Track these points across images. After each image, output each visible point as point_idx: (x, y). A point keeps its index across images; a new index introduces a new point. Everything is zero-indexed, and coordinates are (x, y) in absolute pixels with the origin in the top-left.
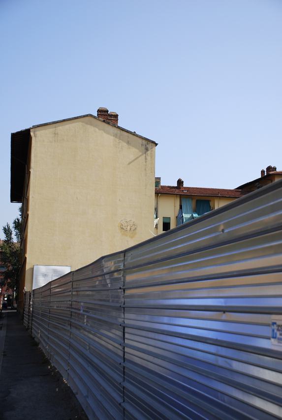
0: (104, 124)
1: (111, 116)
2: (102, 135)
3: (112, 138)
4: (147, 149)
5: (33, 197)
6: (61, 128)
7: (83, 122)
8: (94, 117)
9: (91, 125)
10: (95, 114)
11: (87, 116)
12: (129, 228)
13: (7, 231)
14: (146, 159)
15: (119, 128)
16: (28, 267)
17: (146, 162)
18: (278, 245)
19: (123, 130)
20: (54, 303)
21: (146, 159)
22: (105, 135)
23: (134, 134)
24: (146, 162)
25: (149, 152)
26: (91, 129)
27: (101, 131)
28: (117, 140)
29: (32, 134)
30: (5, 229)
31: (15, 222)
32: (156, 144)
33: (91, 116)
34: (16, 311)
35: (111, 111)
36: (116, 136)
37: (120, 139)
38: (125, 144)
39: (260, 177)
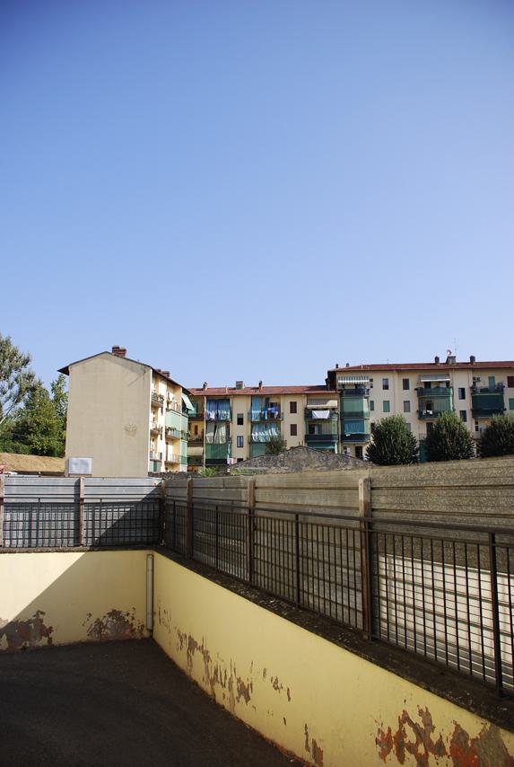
2: (114, 367)
3: (120, 367)
36: (123, 365)
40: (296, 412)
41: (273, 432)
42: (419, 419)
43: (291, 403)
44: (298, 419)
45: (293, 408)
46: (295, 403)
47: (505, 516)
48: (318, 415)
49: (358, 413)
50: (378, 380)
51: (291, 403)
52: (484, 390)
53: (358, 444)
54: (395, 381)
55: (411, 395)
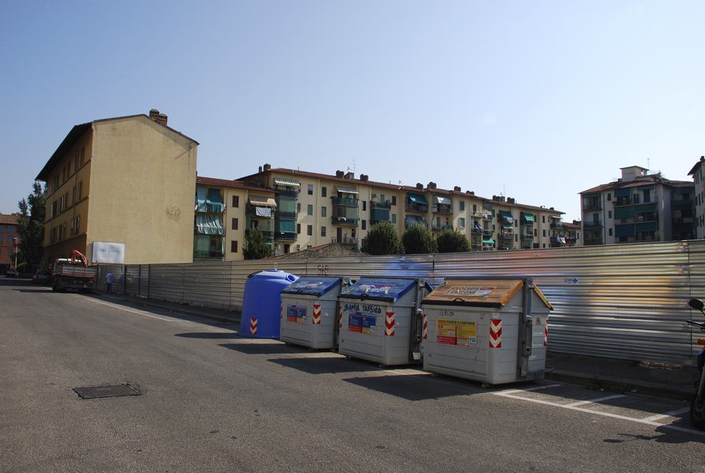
0: (155, 123)
1: (162, 117)
2: (153, 134)
3: (162, 135)
4: (190, 148)
5: (92, 183)
6: (118, 124)
7: (138, 120)
8: (147, 117)
9: (145, 123)
10: (148, 114)
11: (142, 115)
12: (174, 212)
13: (22, 206)
14: (189, 155)
15: (168, 127)
16: (88, 243)
17: (189, 158)
18: (269, 228)
19: (171, 130)
20: (685, 284)
21: (189, 155)
22: (156, 133)
23: (180, 134)
24: (189, 158)
25: (192, 150)
26: (144, 127)
27: (153, 129)
28: (166, 138)
29: (93, 127)
30: (20, 204)
31: (29, 198)
32: (198, 144)
33: (145, 115)
34: (31, 279)
35: (471, 191)
36: (165, 134)
37: (168, 137)
38: (172, 142)
39: (258, 172)
40: (238, 207)
41: (216, 225)
42: (332, 223)
43: (234, 197)
44: (239, 213)
45: (235, 203)
46: (238, 197)
47: (284, 297)
48: (260, 212)
49: (290, 213)
50: (304, 186)
51: (234, 197)
52: (378, 205)
53: (287, 241)
54: (317, 187)
55: (327, 202)
